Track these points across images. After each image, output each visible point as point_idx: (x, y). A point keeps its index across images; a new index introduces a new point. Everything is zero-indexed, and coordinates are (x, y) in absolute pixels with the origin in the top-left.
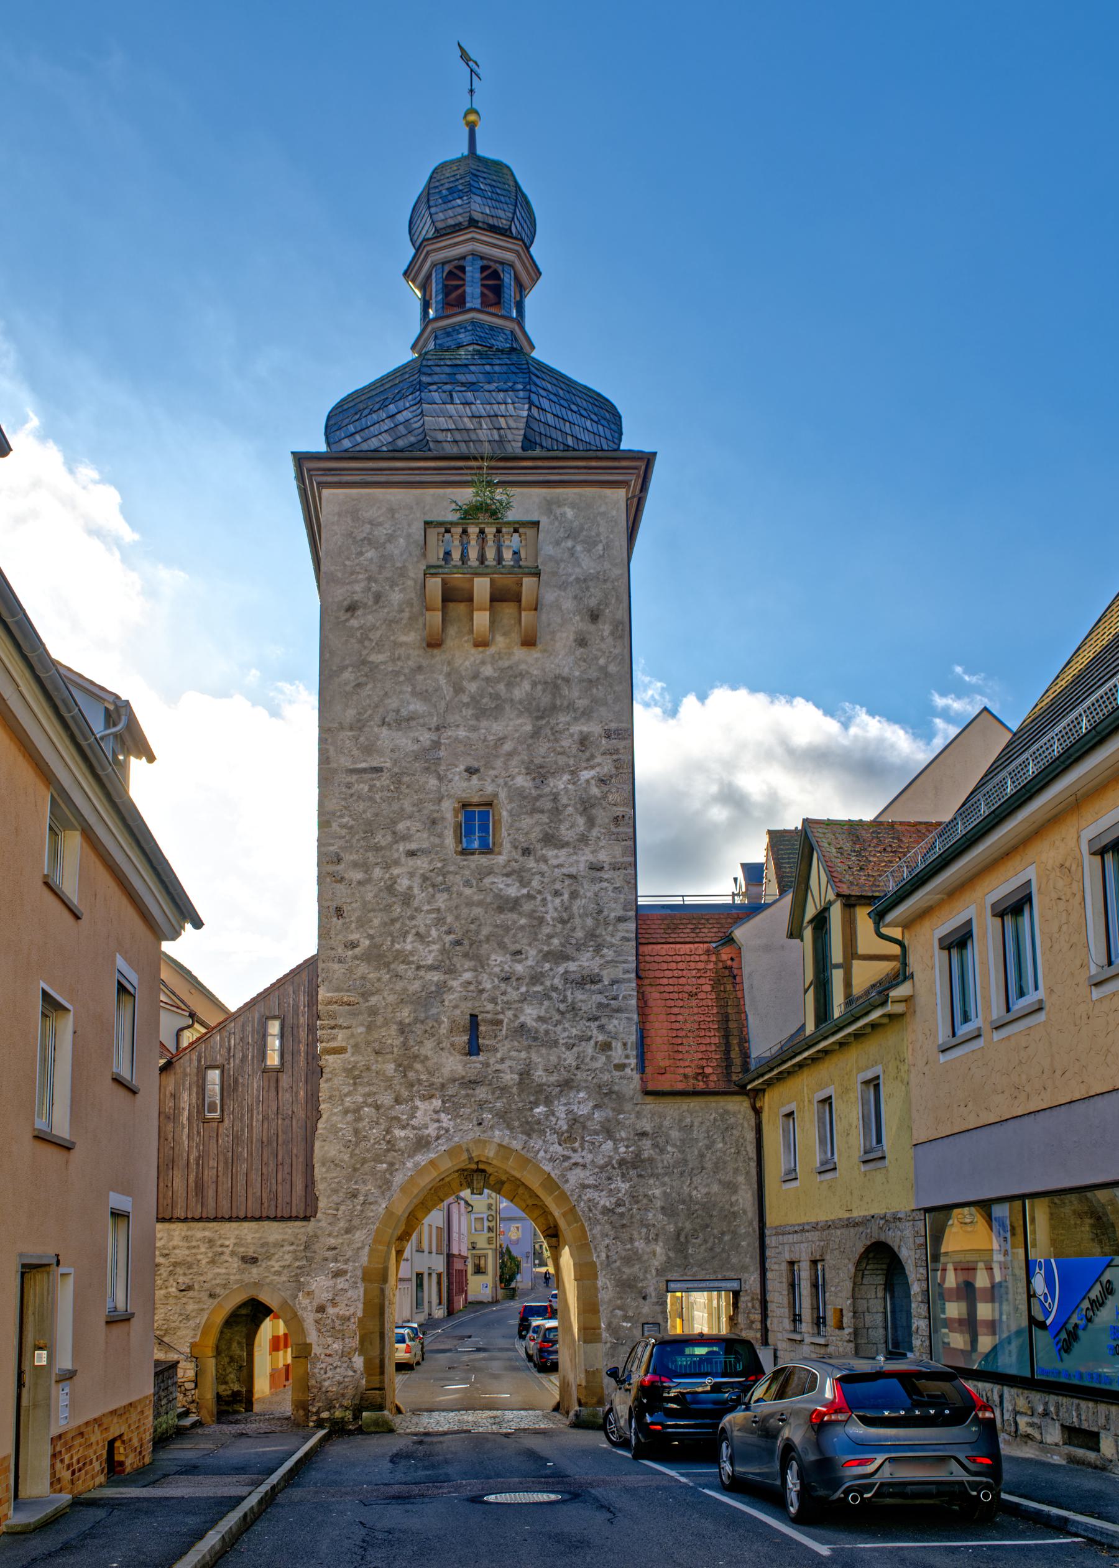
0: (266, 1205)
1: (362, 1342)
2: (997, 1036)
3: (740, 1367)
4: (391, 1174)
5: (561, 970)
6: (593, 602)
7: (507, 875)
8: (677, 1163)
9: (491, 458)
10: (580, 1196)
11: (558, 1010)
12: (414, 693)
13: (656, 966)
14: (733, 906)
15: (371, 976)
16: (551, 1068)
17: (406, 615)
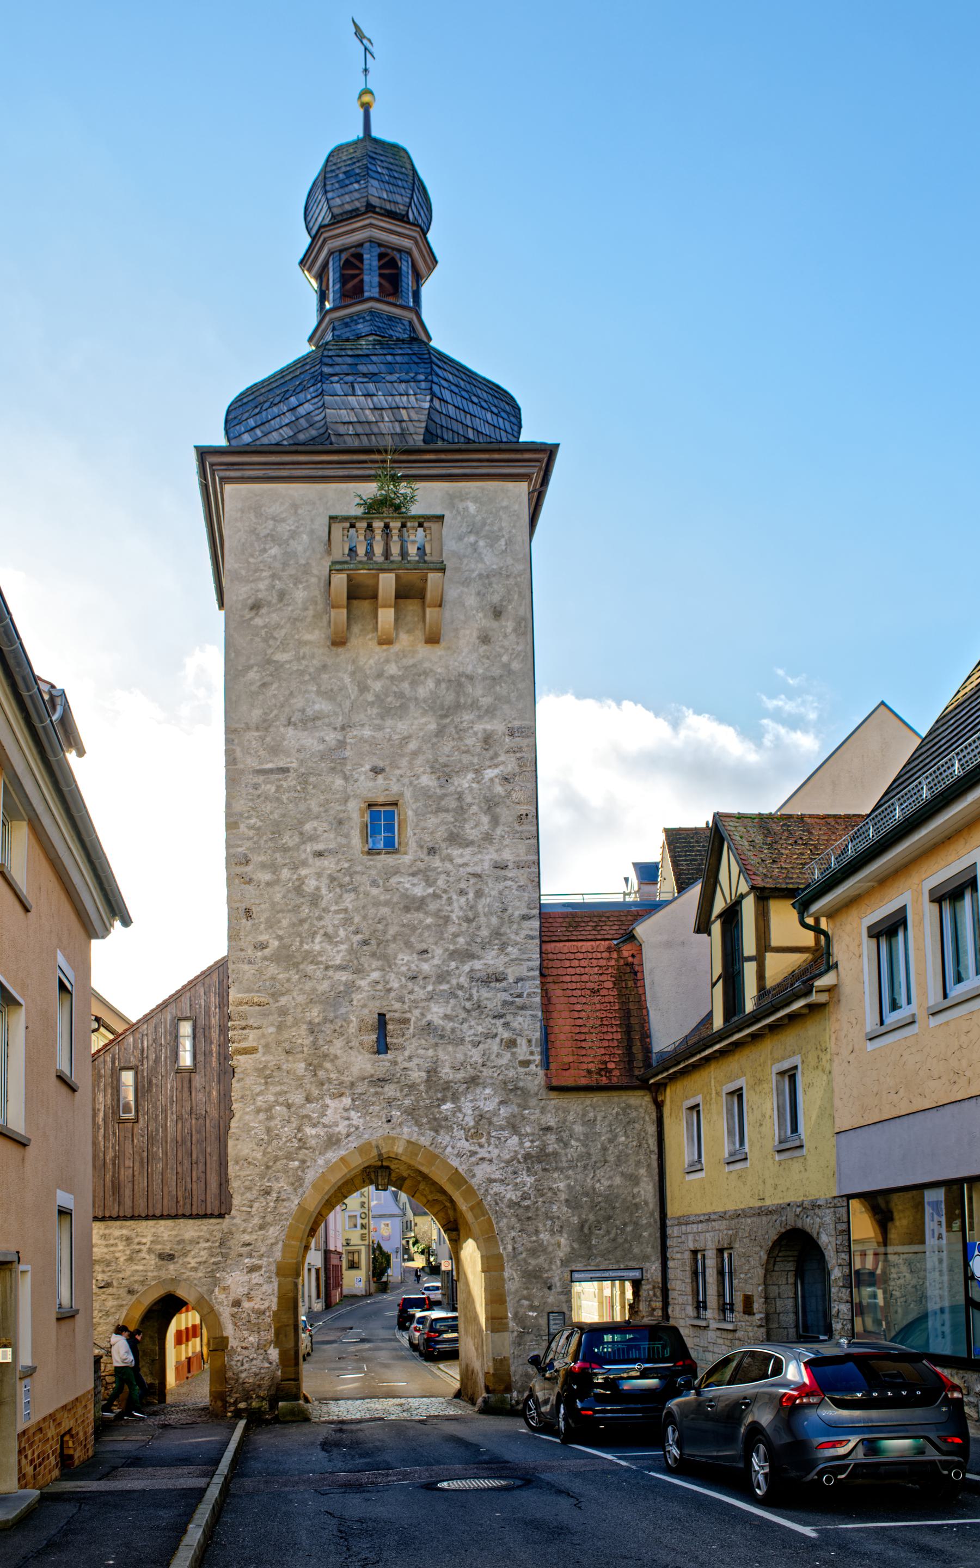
0: (181, 1203)
1: (277, 1334)
2: (934, 1021)
3: (667, 1353)
4: (303, 1171)
5: (467, 968)
6: (496, 599)
7: (413, 875)
8: (581, 1157)
9: (395, 452)
10: (487, 1190)
11: (464, 1008)
12: (319, 693)
13: (558, 964)
14: (624, 904)
15: (281, 976)
16: (458, 1065)
17: (311, 613)
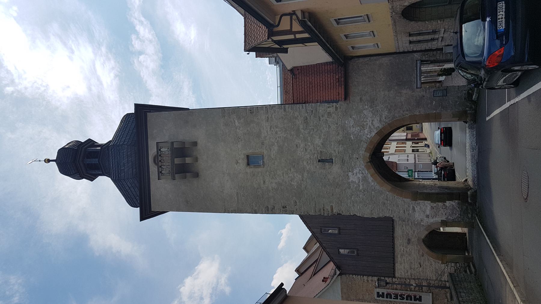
7: (271, 150)
